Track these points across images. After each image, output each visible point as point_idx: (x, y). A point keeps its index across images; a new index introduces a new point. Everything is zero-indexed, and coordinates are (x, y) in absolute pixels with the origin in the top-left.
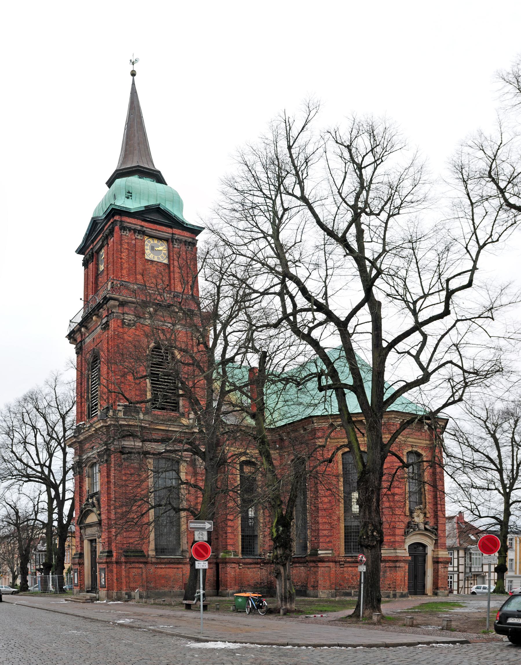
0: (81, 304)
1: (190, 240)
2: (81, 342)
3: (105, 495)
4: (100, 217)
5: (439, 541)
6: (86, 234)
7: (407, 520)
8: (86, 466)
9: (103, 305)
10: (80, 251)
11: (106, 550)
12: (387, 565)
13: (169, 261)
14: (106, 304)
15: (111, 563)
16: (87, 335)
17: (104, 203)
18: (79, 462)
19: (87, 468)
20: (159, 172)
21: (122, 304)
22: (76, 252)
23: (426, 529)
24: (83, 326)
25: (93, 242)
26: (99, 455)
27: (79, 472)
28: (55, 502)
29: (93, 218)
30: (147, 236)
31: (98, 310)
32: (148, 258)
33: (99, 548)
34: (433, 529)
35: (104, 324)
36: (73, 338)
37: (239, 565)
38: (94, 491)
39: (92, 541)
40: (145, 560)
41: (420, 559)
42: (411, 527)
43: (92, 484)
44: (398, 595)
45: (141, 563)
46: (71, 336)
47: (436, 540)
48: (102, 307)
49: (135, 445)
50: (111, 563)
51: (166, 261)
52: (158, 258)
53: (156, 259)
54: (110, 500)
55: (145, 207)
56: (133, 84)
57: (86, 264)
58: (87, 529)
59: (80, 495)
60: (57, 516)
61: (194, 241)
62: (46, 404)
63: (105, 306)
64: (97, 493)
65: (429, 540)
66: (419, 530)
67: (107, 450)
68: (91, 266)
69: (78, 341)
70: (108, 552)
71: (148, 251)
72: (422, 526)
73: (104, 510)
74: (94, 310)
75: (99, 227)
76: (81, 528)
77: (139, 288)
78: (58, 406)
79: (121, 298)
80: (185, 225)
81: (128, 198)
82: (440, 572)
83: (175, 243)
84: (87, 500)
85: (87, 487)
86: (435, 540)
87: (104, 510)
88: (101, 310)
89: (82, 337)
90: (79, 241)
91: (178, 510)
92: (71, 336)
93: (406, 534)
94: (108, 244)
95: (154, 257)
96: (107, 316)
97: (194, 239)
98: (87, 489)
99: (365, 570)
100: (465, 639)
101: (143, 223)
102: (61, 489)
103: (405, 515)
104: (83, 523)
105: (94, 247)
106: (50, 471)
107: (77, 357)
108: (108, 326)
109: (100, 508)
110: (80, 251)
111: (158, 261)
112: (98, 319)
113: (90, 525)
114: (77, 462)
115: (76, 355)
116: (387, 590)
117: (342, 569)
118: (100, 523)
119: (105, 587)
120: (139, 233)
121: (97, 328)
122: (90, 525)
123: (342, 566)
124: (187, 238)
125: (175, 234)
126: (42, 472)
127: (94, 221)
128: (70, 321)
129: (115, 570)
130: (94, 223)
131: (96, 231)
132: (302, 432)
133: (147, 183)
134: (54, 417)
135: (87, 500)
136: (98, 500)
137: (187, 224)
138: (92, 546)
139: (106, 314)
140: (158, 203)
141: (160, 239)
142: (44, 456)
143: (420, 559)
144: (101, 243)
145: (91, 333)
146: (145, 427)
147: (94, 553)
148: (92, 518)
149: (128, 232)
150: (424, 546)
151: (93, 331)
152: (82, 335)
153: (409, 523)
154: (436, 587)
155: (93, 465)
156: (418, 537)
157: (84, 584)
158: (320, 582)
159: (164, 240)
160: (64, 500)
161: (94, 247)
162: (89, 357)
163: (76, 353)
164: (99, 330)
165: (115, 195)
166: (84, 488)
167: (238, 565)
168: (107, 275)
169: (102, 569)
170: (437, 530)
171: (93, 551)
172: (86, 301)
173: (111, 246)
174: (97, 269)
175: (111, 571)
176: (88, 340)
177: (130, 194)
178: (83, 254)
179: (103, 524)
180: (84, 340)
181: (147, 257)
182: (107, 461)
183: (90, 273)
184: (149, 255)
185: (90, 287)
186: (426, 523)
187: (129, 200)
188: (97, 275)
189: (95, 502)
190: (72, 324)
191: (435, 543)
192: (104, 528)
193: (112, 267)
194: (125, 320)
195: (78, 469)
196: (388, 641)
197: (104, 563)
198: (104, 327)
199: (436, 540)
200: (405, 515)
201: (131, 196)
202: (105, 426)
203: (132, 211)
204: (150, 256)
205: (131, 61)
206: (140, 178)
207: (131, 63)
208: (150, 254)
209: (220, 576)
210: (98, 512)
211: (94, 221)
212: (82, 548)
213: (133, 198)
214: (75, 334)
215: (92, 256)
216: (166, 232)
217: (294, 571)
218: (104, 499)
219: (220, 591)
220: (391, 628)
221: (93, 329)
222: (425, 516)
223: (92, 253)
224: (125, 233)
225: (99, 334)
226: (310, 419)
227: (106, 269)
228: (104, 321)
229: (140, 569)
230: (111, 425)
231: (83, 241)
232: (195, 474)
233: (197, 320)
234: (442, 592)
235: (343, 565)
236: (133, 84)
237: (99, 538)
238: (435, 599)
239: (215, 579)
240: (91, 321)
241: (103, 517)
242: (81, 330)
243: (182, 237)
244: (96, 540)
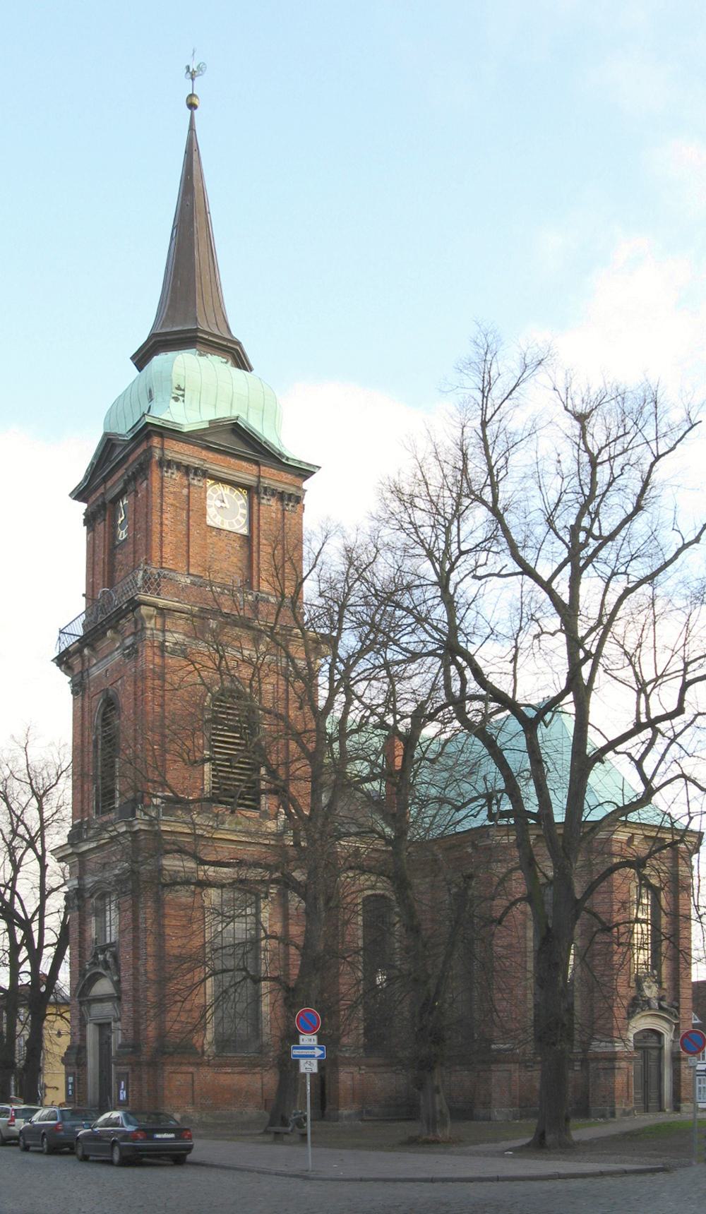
1: (292, 490)
2: (82, 672)
4: (120, 435)
5: (681, 1027)
6: (92, 464)
7: (633, 993)
8: (91, 897)
12: (601, 1065)
13: (250, 530)
16: (95, 661)
17: (129, 391)
19: (93, 900)
20: (238, 343)
22: (70, 495)
24: (87, 645)
25: (105, 480)
28: (24, 953)
33: (117, 1039)
34: (673, 1007)
35: (128, 648)
37: (360, 1069)
38: (105, 940)
39: (103, 1027)
40: (198, 1061)
43: (102, 929)
45: (191, 1064)
46: (63, 660)
47: (677, 1025)
49: (183, 867)
51: (245, 531)
52: (231, 524)
54: (139, 959)
55: (210, 422)
56: (192, 129)
57: (90, 520)
58: (93, 1005)
59: (80, 947)
61: (300, 493)
63: (130, 615)
64: (111, 945)
65: (666, 1025)
66: (650, 1009)
68: (100, 527)
69: (76, 671)
71: (211, 511)
72: (655, 1003)
73: (126, 974)
74: (109, 619)
75: (118, 454)
76: (81, 1003)
77: (193, 583)
78: (31, 780)
80: (284, 460)
81: (176, 399)
82: (683, 1075)
83: (262, 495)
84: (95, 956)
86: (675, 1024)
87: (126, 974)
89: (83, 664)
91: (257, 980)
92: (63, 660)
93: (630, 1015)
94: (136, 492)
97: (299, 488)
98: (94, 936)
101: (204, 454)
102: (35, 926)
105: (106, 491)
106: (14, 893)
107: (74, 699)
108: (137, 652)
109: (118, 970)
110: (80, 494)
112: (115, 636)
113: (100, 1000)
114: (75, 889)
115: (71, 696)
117: (529, 1074)
118: (117, 998)
119: (127, 1105)
120: (195, 474)
121: (113, 652)
123: (530, 1069)
124: (286, 486)
125: (264, 477)
127: (109, 440)
128: (61, 632)
130: (109, 444)
131: (111, 462)
132: (470, 850)
133: (215, 365)
135: (95, 956)
136: (115, 957)
137: (288, 459)
138: (101, 1034)
139: (133, 630)
140: (235, 414)
141: (235, 485)
143: (654, 1053)
144: (121, 486)
145: (102, 659)
148: (104, 987)
149: (175, 472)
150: (659, 1035)
151: (106, 657)
153: (635, 999)
155: (103, 896)
156: (649, 1020)
159: (243, 488)
160: (41, 946)
161: (106, 491)
162: (98, 702)
164: (117, 656)
165: (150, 391)
166: (87, 935)
167: (357, 1069)
170: (678, 1008)
171: (104, 1044)
173: (143, 496)
174: (114, 536)
176: (95, 672)
177: (181, 393)
178: (84, 500)
179: (124, 997)
182: (133, 891)
184: (214, 518)
185: (99, 568)
187: (180, 404)
188: (113, 546)
189: (110, 960)
191: (675, 1030)
192: (126, 1007)
193: (144, 540)
195: (76, 901)
198: (129, 654)
199: (677, 1025)
200: (629, 987)
201: (183, 396)
202: (130, 832)
203: (185, 430)
204: (216, 520)
205: (188, 68)
206: (200, 355)
207: (189, 75)
208: (215, 516)
210: (115, 978)
211: (109, 440)
212: (83, 1038)
213: (185, 399)
215: (103, 506)
216: (246, 473)
217: (453, 1079)
218: (126, 957)
221: (107, 652)
222: (660, 987)
224: (169, 474)
225: (118, 664)
227: (131, 541)
228: (128, 642)
229: (190, 1075)
231: (86, 477)
232: (286, 917)
233: (297, 651)
235: (531, 1067)
236: (192, 129)
237: (115, 1022)
238: (676, 1117)
239: (319, 1092)
241: (125, 986)
242: (83, 651)
243: (278, 484)
244: (109, 1024)
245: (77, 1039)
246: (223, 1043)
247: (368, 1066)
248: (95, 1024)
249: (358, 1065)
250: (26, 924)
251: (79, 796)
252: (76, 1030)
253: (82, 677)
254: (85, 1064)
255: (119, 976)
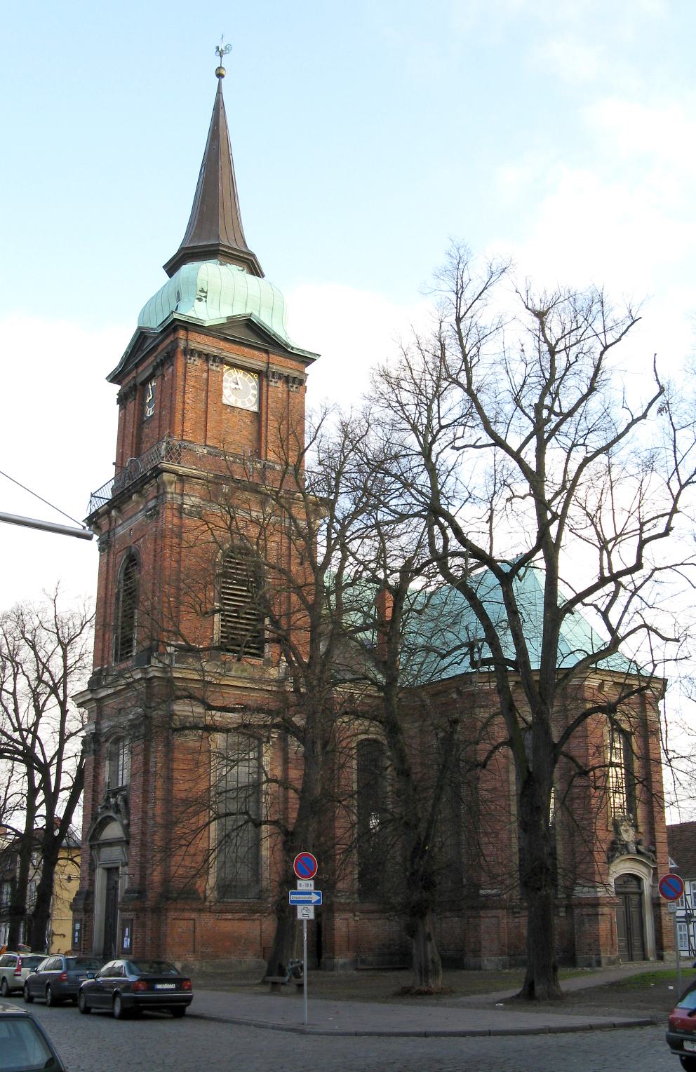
0: (111, 472)
1: (296, 374)
3: (139, 793)
7: (611, 837)
8: (106, 741)
9: (151, 480)
10: (115, 378)
11: (136, 887)
13: (260, 407)
14: (156, 477)
15: (143, 910)
16: (121, 522)
18: (95, 734)
19: (108, 744)
20: (253, 255)
21: (182, 478)
23: (639, 852)
25: (137, 366)
26: (133, 725)
27: (94, 751)
29: (139, 328)
30: (227, 364)
31: (142, 486)
32: (228, 403)
33: (124, 884)
34: (650, 851)
35: (150, 510)
36: (95, 523)
37: (355, 915)
38: (117, 784)
39: (111, 871)
41: (635, 898)
42: (616, 849)
43: (115, 773)
44: (604, 961)
45: (193, 910)
47: (655, 869)
48: (148, 482)
49: (193, 712)
50: (143, 910)
51: (255, 409)
53: (239, 405)
55: (228, 318)
56: (219, 92)
57: (122, 400)
59: (94, 791)
60: (44, 822)
62: (37, 623)
63: (153, 482)
64: (123, 788)
65: (645, 870)
66: (629, 853)
67: (146, 717)
69: (104, 530)
70: (139, 892)
72: (632, 847)
73: (135, 817)
75: (149, 344)
77: (209, 453)
78: (58, 630)
79: (181, 470)
80: (289, 350)
84: (107, 799)
85: (107, 776)
88: (146, 487)
90: (114, 362)
93: (610, 860)
94: (163, 376)
95: (236, 401)
96: (156, 497)
97: (302, 373)
98: (107, 780)
99: (312, 916)
100: (649, 1019)
103: (607, 830)
104: (97, 839)
106: (35, 737)
107: (100, 556)
108: (158, 513)
109: (128, 814)
110: (115, 378)
111: (242, 407)
112: (140, 499)
113: (110, 844)
116: (587, 954)
117: (517, 920)
118: (126, 842)
119: (131, 953)
121: (137, 513)
122: (110, 844)
123: (517, 915)
126: (23, 743)
127: (142, 333)
128: (92, 496)
129: (149, 923)
130: (141, 337)
131: (143, 351)
132: (454, 696)
134: (48, 644)
135: (107, 799)
136: (126, 800)
137: (293, 348)
138: (109, 878)
140: (249, 311)
142: (28, 718)
143: (635, 898)
144: (151, 370)
146: (210, 682)
147: (113, 891)
148: (113, 831)
151: (131, 518)
152: (110, 521)
153: (613, 843)
154: (660, 946)
155: (117, 741)
157: (91, 947)
158: (484, 943)
159: (255, 372)
160: (58, 790)
162: (121, 559)
163: (99, 550)
164: (140, 517)
165: (178, 293)
166: (101, 778)
167: (351, 915)
168: (160, 427)
169: (128, 920)
170: (654, 852)
171: (112, 889)
172: (119, 464)
173: (168, 379)
175: (143, 925)
176: (120, 531)
177: (204, 294)
178: (119, 383)
180: (114, 529)
181: (225, 401)
182: (145, 736)
183: (130, 419)
184: (229, 398)
185: (128, 441)
186: (638, 843)
187: (203, 303)
188: (141, 422)
189: (121, 803)
190: (94, 500)
191: (654, 874)
193: (168, 416)
194: (185, 506)
195: (92, 745)
196: (552, 1025)
197: (130, 911)
198: (151, 515)
200: (607, 830)
201: (206, 297)
203: (206, 325)
205: (218, 48)
206: (221, 264)
207: (218, 53)
208: (230, 396)
209: (323, 934)
210: (125, 822)
211: (142, 333)
212: (92, 883)
214: (99, 518)
216: (257, 360)
217: (443, 925)
218: (136, 800)
219: (323, 960)
220: (569, 1010)
221: (131, 513)
223: (135, 385)
225: (141, 524)
226: (468, 676)
227: (157, 417)
228: (151, 504)
229: (192, 922)
230: (154, 677)
231: (121, 363)
234: (671, 955)
235: (519, 913)
236: (219, 92)
237: (123, 866)
239: (316, 939)
240: (129, 501)
241: (134, 830)
243: (283, 369)
244: (117, 868)
245: (86, 883)
246: (225, 888)
247: (362, 912)
248: (104, 868)
249: (353, 911)
250: (44, 769)
251: (100, 645)
252: (86, 874)
253: (109, 535)
254: (92, 911)
255: (129, 820)
